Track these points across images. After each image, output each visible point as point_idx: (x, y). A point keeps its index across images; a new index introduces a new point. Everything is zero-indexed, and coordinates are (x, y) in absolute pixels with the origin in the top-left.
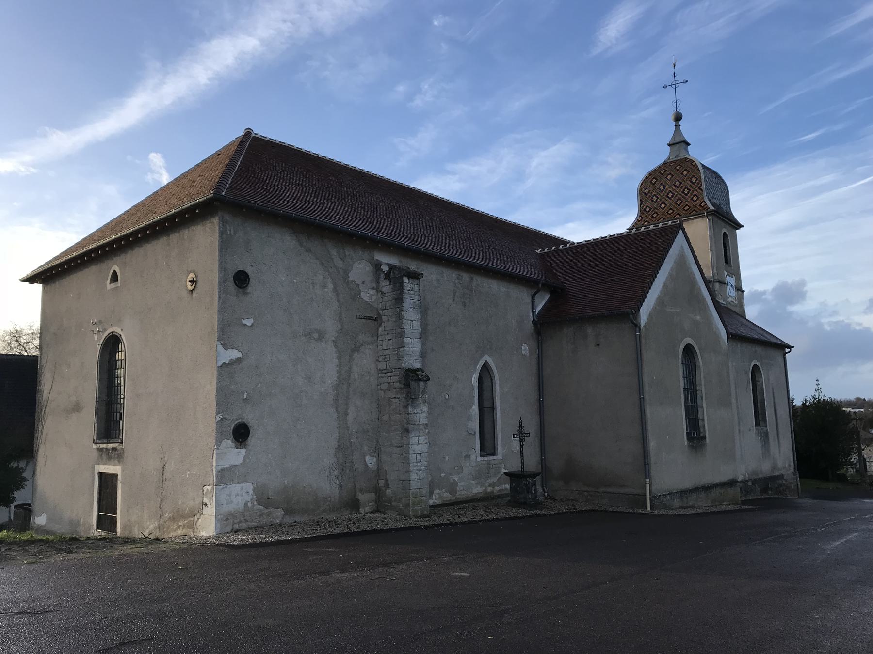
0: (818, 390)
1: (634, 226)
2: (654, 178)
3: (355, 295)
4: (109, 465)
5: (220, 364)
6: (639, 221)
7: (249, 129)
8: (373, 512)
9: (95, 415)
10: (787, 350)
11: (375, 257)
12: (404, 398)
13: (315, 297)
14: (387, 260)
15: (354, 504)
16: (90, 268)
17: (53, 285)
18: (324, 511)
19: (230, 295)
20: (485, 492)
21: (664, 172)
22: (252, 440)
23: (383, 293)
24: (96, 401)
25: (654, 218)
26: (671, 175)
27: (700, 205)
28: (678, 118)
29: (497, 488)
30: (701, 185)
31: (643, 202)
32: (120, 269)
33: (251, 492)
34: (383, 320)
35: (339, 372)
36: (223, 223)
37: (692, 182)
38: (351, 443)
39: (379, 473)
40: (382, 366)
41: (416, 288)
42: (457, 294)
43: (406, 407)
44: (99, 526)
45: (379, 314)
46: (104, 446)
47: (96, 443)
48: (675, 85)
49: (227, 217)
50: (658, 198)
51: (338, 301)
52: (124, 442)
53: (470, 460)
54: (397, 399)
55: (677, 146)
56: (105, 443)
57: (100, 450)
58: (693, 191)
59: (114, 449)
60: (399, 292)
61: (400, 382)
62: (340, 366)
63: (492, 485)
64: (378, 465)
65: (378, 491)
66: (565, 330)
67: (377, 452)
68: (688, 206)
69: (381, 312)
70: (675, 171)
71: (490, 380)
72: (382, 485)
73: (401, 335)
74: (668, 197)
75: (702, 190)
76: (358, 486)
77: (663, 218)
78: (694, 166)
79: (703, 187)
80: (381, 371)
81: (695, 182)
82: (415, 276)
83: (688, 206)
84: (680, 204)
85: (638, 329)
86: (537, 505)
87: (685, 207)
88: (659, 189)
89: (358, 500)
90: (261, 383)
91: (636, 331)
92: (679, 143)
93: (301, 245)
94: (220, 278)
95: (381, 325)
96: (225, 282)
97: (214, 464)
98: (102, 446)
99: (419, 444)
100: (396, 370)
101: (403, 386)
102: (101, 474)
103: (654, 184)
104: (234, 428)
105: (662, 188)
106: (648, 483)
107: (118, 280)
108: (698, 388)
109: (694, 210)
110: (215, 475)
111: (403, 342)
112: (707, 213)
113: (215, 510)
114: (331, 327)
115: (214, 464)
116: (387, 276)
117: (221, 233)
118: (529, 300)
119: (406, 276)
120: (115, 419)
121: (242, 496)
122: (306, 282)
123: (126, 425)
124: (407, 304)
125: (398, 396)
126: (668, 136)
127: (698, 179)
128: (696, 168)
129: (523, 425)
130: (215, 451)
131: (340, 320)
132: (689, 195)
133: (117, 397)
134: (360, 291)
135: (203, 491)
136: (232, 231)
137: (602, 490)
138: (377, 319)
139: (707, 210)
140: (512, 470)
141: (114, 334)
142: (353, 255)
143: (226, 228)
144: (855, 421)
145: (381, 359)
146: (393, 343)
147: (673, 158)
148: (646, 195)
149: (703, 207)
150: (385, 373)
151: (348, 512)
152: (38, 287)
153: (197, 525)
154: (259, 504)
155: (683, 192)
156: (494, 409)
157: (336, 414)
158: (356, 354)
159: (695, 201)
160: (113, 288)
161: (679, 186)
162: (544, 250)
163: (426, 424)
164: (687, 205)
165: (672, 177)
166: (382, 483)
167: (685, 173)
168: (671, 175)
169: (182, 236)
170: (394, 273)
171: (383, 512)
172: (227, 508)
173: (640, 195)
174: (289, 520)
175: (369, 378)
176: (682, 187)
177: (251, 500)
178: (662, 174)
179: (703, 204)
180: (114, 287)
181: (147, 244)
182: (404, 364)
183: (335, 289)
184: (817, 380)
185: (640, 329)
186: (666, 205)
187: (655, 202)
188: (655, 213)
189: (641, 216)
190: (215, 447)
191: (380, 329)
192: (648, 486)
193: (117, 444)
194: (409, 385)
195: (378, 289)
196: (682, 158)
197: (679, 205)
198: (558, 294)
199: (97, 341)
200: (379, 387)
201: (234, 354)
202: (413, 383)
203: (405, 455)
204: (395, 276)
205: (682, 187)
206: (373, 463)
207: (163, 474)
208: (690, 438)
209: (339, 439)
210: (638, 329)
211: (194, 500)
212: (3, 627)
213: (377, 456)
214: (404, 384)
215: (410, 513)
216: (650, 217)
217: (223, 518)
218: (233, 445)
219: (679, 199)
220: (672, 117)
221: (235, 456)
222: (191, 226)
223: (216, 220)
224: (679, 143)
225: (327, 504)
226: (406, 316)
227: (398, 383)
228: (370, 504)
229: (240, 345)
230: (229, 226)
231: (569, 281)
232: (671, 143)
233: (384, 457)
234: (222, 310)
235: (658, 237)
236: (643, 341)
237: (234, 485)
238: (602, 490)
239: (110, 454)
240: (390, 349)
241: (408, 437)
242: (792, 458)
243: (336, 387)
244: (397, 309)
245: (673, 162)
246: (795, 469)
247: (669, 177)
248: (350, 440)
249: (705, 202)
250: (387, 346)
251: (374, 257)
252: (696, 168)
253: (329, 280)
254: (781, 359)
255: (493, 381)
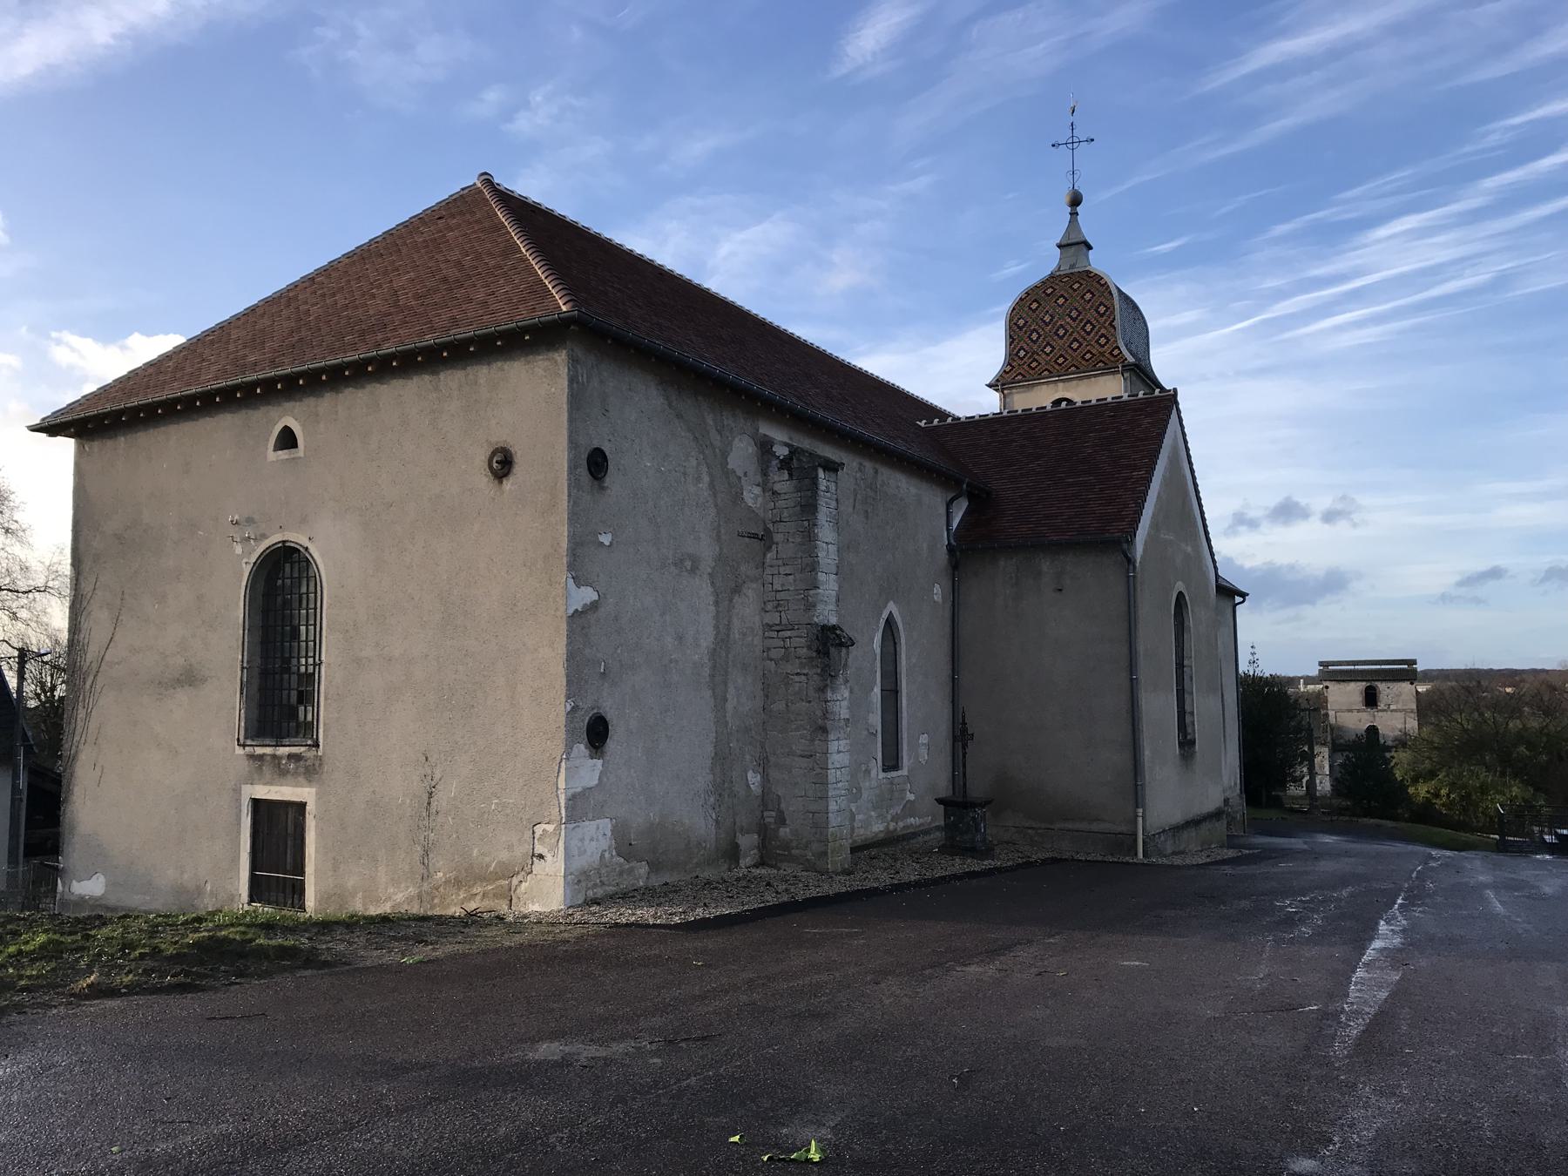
0: (1254, 662)
1: (997, 380)
2: (1035, 301)
3: (737, 497)
4: (281, 785)
5: (571, 611)
6: (1008, 373)
7: (486, 174)
8: (756, 866)
9: (241, 693)
10: (1238, 599)
11: (761, 431)
12: (817, 674)
13: (687, 497)
14: (780, 437)
15: (732, 853)
16: (216, 419)
17: (109, 443)
18: (698, 865)
19: (583, 492)
20: (887, 830)
21: (1052, 292)
22: (611, 745)
23: (774, 493)
24: (243, 668)
25: (1033, 369)
26: (1064, 297)
27: (1111, 353)
28: (1076, 201)
29: (901, 824)
30: (1114, 319)
31: (1014, 340)
32: (303, 426)
33: (609, 834)
34: (775, 540)
35: (716, 627)
36: (574, 361)
37: (1099, 313)
38: (730, 747)
39: (767, 799)
40: (768, 619)
41: (833, 487)
42: (859, 497)
43: (822, 690)
44: (258, 890)
45: (766, 530)
46: (268, 750)
47: (244, 746)
48: (1072, 143)
49: (579, 353)
50: (1040, 336)
51: (716, 506)
52: (321, 744)
53: (870, 776)
54: (803, 677)
55: (1073, 249)
56: (269, 746)
57: (251, 757)
58: (1100, 328)
59: (295, 758)
60: (809, 493)
61: (809, 648)
62: (717, 617)
63: (895, 819)
64: (763, 787)
65: (764, 832)
66: (1002, 563)
67: (763, 765)
68: (1091, 353)
69: (770, 526)
70: (1071, 291)
71: (892, 643)
72: (772, 820)
73: (813, 567)
74: (1058, 335)
75: (1115, 328)
76: (738, 824)
77: (1049, 371)
78: (1103, 285)
79: (1117, 323)
80: (769, 627)
81: (1104, 313)
82: (832, 467)
83: (1091, 353)
84: (1077, 349)
85: (1131, 567)
86: (988, 852)
87: (1085, 355)
88: (1042, 319)
89: (737, 846)
90: (622, 646)
91: (1128, 569)
92: (1075, 244)
93: (670, 406)
94: (570, 461)
95: (771, 547)
96: (576, 467)
97: (562, 785)
98: (259, 751)
99: (839, 752)
100: (800, 626)
101: (814, 654)
102: (257, 804)
103: (1034, 311)
104: (588, 723)
105: (1047, 318)
106: (1141, 814)
107: (297, 444)
108: (1186, 662)
109: (1101, 361)
110: (563, 805)
111: (816, 579)
112: (1123, 366)
113: (563, 866)
114: (706, 551)
115: (562, 785)
116: (785, 464)
117: (572, 380)
118: (943, 510)
119: (822, 467)
120: (285, 702)
121: (597, 840)
122: (676, 471)
123: (327, 711)
124: (823, 515)
125: (805, 672)
126: (1058, 233)
127: (1110, 309)
128: (1106, 289)
129: (966, 721)
130: (563, 764)
131: (718, 538)
132: (1092, 335)
133: (299, 662)
134: (742, 489)
135: (534, 833)
136: (585, 376)
137: (1058, 826)
138: (764, 539)
139: (1123, 362)
140: (941, 796)
141: (288, 544)
142: (733, 425)
143: (577, 372)
144: (1307, 712)
145: (769, 607)
146: (795, 581)
147: (1065, 269)
148: (1020, 328)
149: (1116, 356)
150: (778, 631)
151: (726, 866)
152: (66, 447)
153: (518, 891)
154: (619, 855)
155: (1083, 328)
156: (897, 692)
157: (713, 700)
158: (736, 599)
159: (1103, 346)
160: (282, 460)
161: (1076, 318)
162: (932, 422)
163: (848, 720)
164: (1089, 352)
165: (1065, 302)
166: (770, 817)
167: (1088, 296)
168: (1064, 297)
169: (471, 377)
170: (799, 460)
171: (772, 866)
172: (580, 863)
173: (1010, 328)
174: (656, 881)
175: (753, 640)
176: (1081, 321)
177: (609, 847)
178: (1048, 295)
179: (1116, 352)
180: (287, 457)
181: (378, 385)
182: (817, 617)
183: (712, 485)
184: (1252, 647)
185: (1135, 567)
186: (1053, 348)
187: (1035, 342)
188: (1035, 360)
189: (1009, 364)
190: (564, 756)
191: (769, 555)
192: (1140, 819)
193: (303, 749)
194: (829, 653)
195: (765, 486)
196: (1080, 270)
197: (1075, 350)
198: (981, 501)
199: (240, 557)
200: (765, 654)
201: (588, 595)
202: (832, 650)
203: (819, 771)
204: (801, 468)
205: (1081, 321)
206: (756, 784)
207: (429, 804)
208: (1181, 744)
209: (716, 742)
210: (1131, 567)
211: (510, 847)
212: (7, 1084)
213: (762, 771)
214: (818, 652)
215: (829, 866)
216: (1025, 367)
217: (577, 879)
218: (587, 752)
219: (1075, 340)
220: (1065, 199)
221: (590, 771)
222: (497, 360)
223: (561, 357)
224: (1075, 244)
225: (702, 853)
226: (820, 535)
227: (805, 650)
228: (752, 853)
229: (596, 579)
230: (582, 369)
231: (996, 479)
232: (1065, 242)
233: (774, 774)
234: (574, 517)
235: (1140, 415)
236: (1138, 585)
237: (587, 823)
238: (1058, 826)
239: (282, 767)
240: (788, 590)
241: (826, 741)
242: (1238, 771)
243: (713, 653)
244: (806, 523)
245: (1066, 276)
246: (1241, 789)
247: (1061, 301)
248: (729, 744)
249: (1120, 349)
250: (783, 585)
251: (758, 430)
252: (1106, 289)
253: (704, 469)
254: (1230, 610)
255: (897, 646)
